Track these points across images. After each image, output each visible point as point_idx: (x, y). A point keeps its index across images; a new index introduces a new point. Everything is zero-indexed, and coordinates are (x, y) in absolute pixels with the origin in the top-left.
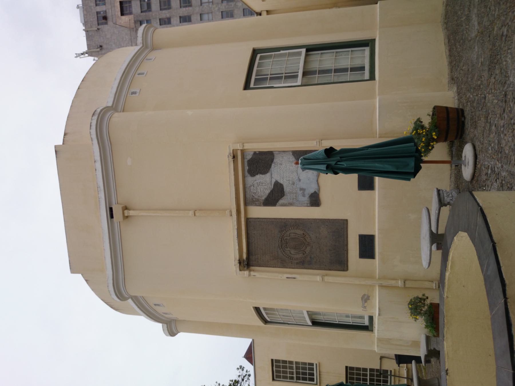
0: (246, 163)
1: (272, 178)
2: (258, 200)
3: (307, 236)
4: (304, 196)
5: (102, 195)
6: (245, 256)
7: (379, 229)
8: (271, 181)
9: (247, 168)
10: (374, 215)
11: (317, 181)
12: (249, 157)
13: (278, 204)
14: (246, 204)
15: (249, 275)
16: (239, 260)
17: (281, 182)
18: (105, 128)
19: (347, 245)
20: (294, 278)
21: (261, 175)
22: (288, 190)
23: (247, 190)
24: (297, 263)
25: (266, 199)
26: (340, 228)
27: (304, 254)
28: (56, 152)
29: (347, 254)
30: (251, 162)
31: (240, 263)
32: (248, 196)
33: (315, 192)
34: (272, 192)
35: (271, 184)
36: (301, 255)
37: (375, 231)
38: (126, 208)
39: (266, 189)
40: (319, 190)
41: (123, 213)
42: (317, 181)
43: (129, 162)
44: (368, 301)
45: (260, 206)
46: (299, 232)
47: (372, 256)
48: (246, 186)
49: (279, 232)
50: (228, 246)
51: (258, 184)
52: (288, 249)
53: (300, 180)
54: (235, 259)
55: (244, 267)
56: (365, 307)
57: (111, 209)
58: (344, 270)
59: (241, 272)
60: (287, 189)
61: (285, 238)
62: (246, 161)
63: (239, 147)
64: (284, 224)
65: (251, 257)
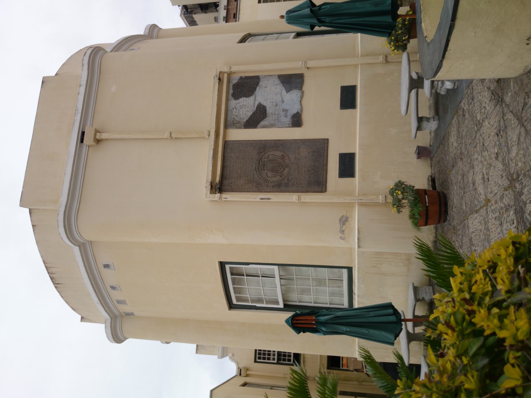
0: (231, 87)
1: (255, 100)
2: (239, 122)
3: (286, 158)
4: (286, 116)
5: (78, 118)
6: (218, 179)
7: (360, 146)
8: (255, 103)
9: (231, 91)
10: (356, 134)
11: (301, 102)
12: (235, 81)
13: (259, 125)
14: (226, 127)
16: (211, 183)
17: (264, 104)
18: (98, 58)
19: (327, 165)
20: (269, 199)
21: (245, 98)
22: (270, 111)
23: (229, 113)
24: (273, 186)
25: (248, 121)
26: (320, 147)
27: (281, 176)
28: (43, 82)
29: (326, 174)
30: (236, 87)
31: (212, 187)
32: (229, 119)
33: (298, 113)
34: (254, 114)
35: (254, 106)
36: (278, 178)
37: (355, 149)
38: (247, 370)
39: (248, 111)
40: (302, 111)
41: (95, 135)
42: (301, 102)
43: (114, 89)
44: (347, 223)
45: (240, 128)
46: (278, 153)
47: (351, 174)
48: (229, 109)
49: (257, 154)
50: (202, 163)
51: (241, 107)
52: (266, 172)
53: (283, 102)
54: (207, 181)
55: (216, 191)
56: (343, 231)
57: (83, 133)
58: (322, 192)
60: (269, 111)
62: (231, 85)
63: (226, 69)
64: (263, 146)
65: (224, 182)
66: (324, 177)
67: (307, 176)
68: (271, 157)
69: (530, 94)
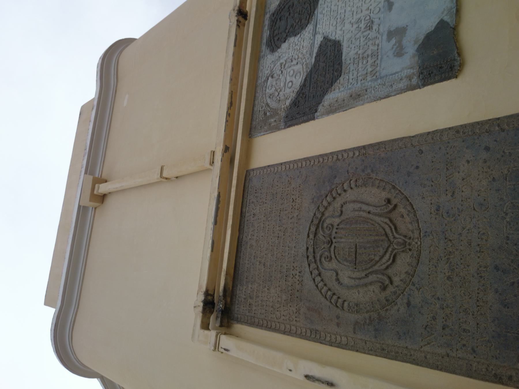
3: (401, 209)
13: (320, 108)
15: (216, 346)
27: (384, 288)
33: (442, 25)
45: (277, 128)
52: (334, 264)
59: (202, 331)
61: (328, 221)
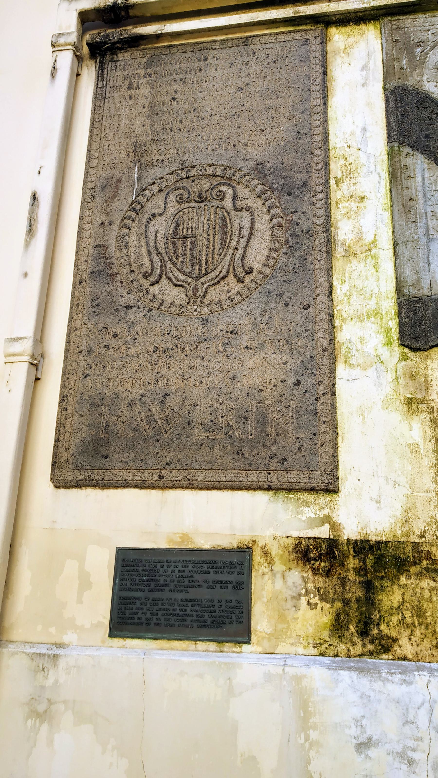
19: (191, 485)
24: (102, 248)
29: (142, 485)
66: (128, 476)
67: (138, 391)
68: (243, 220)
69: (436, 370)
